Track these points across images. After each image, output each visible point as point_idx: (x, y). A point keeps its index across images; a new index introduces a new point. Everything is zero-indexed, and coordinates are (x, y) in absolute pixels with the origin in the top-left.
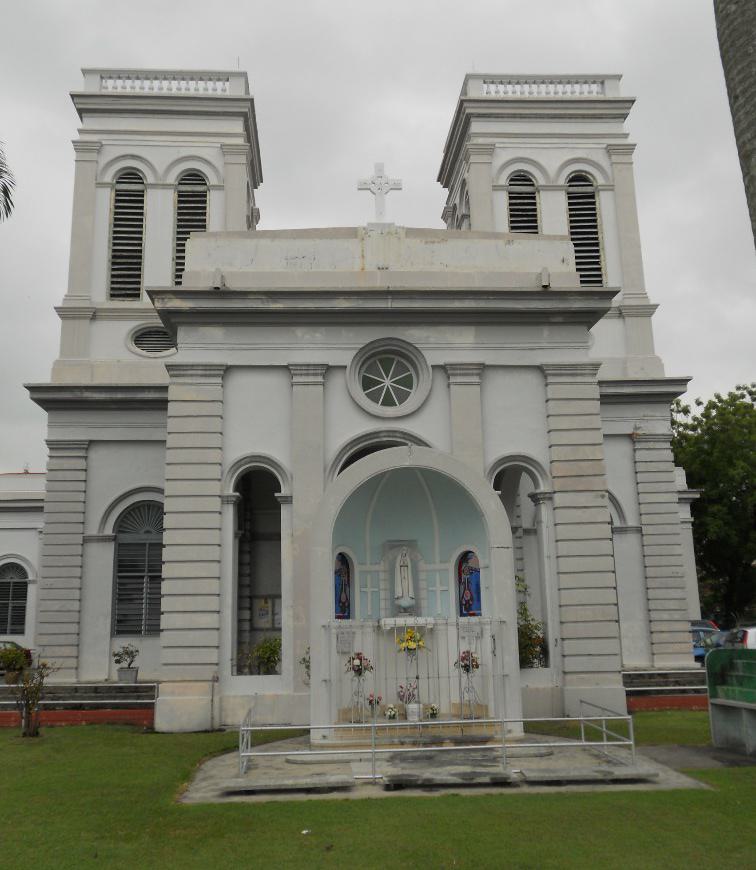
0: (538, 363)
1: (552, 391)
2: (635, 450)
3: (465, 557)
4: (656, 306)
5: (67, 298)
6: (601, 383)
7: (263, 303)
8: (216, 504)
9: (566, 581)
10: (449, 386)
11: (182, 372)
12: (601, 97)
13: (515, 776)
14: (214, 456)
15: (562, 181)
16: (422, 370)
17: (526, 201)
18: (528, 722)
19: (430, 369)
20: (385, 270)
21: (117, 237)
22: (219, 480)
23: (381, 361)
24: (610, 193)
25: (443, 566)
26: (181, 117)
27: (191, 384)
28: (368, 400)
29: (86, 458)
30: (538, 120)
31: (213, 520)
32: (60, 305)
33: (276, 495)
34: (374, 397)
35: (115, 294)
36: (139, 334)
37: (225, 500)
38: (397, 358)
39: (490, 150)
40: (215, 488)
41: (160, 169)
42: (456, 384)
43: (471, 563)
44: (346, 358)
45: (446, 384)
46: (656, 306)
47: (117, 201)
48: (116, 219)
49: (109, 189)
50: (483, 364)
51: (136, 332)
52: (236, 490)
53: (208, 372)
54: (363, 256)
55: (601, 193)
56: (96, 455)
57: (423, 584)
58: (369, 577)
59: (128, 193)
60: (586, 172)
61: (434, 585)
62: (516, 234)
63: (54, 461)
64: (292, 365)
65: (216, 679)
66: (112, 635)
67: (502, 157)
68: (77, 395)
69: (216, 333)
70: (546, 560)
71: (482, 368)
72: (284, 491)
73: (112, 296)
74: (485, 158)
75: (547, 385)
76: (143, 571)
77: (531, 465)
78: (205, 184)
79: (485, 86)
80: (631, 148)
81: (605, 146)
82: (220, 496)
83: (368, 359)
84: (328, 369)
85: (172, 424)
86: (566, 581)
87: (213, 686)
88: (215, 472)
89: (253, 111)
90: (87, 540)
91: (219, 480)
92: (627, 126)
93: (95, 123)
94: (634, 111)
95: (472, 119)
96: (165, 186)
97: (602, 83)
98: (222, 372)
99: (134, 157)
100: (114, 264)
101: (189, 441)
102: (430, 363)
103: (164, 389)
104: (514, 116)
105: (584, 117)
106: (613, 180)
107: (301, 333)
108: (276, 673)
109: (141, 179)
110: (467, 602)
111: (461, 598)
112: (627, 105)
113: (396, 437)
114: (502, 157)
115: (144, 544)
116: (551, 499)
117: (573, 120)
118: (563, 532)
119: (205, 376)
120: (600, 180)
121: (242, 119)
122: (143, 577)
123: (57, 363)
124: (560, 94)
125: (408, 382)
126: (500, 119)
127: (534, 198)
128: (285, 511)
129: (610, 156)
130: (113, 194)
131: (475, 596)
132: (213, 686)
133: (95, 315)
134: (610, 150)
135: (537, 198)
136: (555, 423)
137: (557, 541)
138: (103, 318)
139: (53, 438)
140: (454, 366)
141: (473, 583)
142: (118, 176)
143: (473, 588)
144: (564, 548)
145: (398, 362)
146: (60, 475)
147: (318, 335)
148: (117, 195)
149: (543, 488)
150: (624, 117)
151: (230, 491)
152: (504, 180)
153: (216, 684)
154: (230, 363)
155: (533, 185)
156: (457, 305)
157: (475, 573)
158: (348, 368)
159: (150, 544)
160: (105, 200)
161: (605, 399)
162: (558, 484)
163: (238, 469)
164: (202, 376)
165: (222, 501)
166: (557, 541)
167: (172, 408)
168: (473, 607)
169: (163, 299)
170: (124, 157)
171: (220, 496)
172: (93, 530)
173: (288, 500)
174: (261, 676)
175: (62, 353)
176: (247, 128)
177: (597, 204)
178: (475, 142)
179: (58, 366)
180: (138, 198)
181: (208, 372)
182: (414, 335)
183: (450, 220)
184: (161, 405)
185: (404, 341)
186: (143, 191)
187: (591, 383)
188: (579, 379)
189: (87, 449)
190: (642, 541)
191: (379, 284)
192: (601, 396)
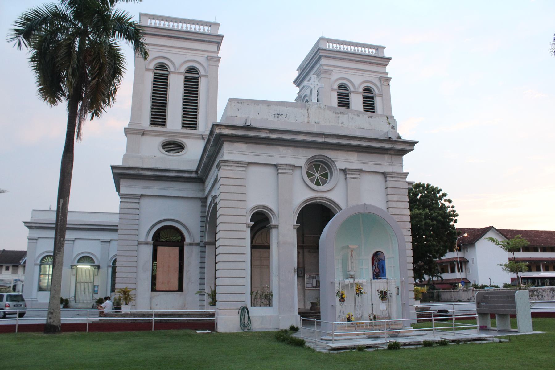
0: (383, 171)
3: (376, 254)
5: (130, 124)
7: (267, 134)
8: (244, 227)
10: (278, 174)
11: (227, 164)
12: (376, 55)
13: (312, 348)
15: (361, 90)
17: (368, 100)
18: (16, 327)
19: (338, 169)
20: (318, 124)
21: (154, 96)
23: (314, 165)
24: (381, 98)
26: (153, 37)
27: (232, 170)
28: (309, 181)
30: (351, 61)
31: (241, 235)
34: (312, 181)
35: (153, 123)
36: (165, 143)
38: (322, 164)
39: (330, 72)
41: (177, 65)
44: (302, 162)
48: (154, 87)
49: (152, 72)
50: (294, 165)
51: (163, 143)
53: (240, 165)
54: (308, 117)
55: (377, 97)
56: (144, 201)
59: (160, 75)
60: (371, 87)
63: (123, 204)
64: (279, 164)
66: (38, 291)
67: (335, 76)
69: (242, 147)
71: (361, 171)
72: (273, 222)
73: (183, 126)
74: (327, 76)
75: (386, 181)
77: (270, 212)
78: (198, 74)
81: (379, 77)
82: (245, 224)
83: (311, 163)
84: (295, 167)
90: (139, 243)
92: (388, 69)
94: (391, 62)
95: (322, 58)
96: (179, 73)
97: (377, 49)
98: (246, 165)
99: (164, 58)
100: (152, 109)
101: (230, 197)
104: (340, 59)
105: (370, 63)
106: (382, 93)
109: (167, 68)
111: (374, 271)
112: (388, 60)
113: (323, 200)
114: (335, 76)
117: (365, 64)
119: (238, 166)
120: (376, 91)
121: (217, 45)
123: (125, 156)
124: (360, 51)
125: (326, 176)
126: (335, 59)
128: (274, 232)
131: (381, 271)
133: (144, 133)
138: (147, 135)
140: (349, 170)
142: (156, 66)
145: (322, 166)
146: (126, 211)
147: (289, 151)
150: (386, 65)
152: (336, 87)
154: (250, 162)
155: (348, 90)
158: (303, 167)
160: (149, 78)
163: (253, 211)
164: (236, 166)
169: (220, 128)
171: (245, 224)
172: (142, 239)
173: (276, 227)
174: (261, 308)
175: (127, 151)
177: (375, 102)
178: (323, 68)
179: (125, 158)
180: (165, 78)
181: (240, 165)
182: (331, 155)
185: (330, 159)
186: (168, 75)
188: (399, 179)
189: (139, 199)
191: (358, 134)
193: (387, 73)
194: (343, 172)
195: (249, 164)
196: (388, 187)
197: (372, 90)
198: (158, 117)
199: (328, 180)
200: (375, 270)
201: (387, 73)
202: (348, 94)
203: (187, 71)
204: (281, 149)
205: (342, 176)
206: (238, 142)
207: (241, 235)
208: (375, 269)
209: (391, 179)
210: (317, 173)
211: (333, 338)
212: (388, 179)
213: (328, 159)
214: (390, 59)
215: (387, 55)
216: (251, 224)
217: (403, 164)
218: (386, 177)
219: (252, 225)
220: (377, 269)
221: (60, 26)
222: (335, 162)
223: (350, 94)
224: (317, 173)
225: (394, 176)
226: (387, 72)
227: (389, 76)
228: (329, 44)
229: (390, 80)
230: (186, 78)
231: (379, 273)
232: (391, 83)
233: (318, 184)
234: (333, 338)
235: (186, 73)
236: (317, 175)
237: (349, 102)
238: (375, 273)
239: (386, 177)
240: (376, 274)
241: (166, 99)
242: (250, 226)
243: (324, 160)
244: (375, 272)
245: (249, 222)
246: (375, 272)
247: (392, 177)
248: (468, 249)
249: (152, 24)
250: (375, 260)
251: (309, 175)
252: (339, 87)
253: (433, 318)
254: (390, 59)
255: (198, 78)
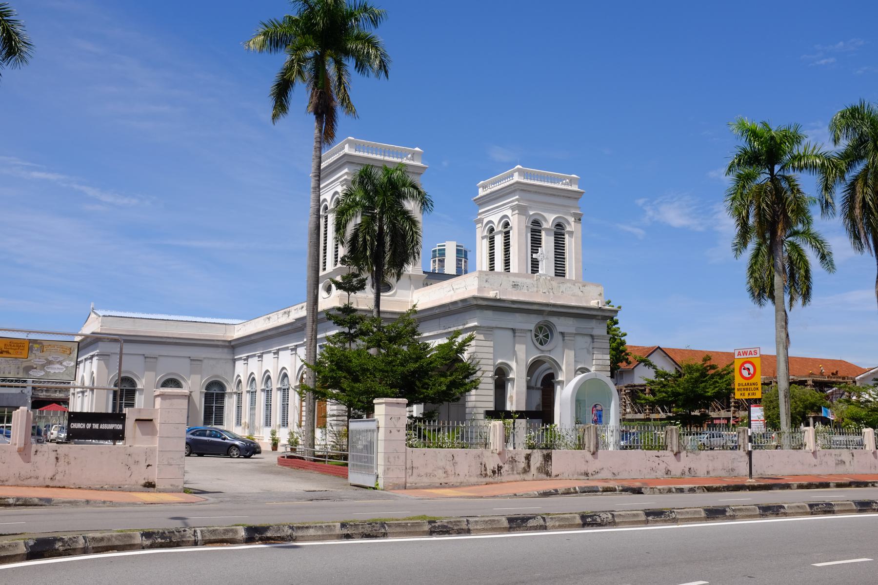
34: (537, 340)
44: (532, 327)
119: (487, 330)
182: (554, 320)
185: (554, 325)
194: (591, 338)
195: (493, 328)
197: (563, 225)
199: (549, 340)
204: (517, 315)
205: (560, 337)
206: (486, 310)
209: (520, 335)
212: (595, 340)
213: (552, 324)
218: (564, 337)
221: (418, 151)
233: (541, 344)
239: (564, 337)
248: (624, 375)
251: (536, 336)
252: (532, 222)
253: (124, 402)
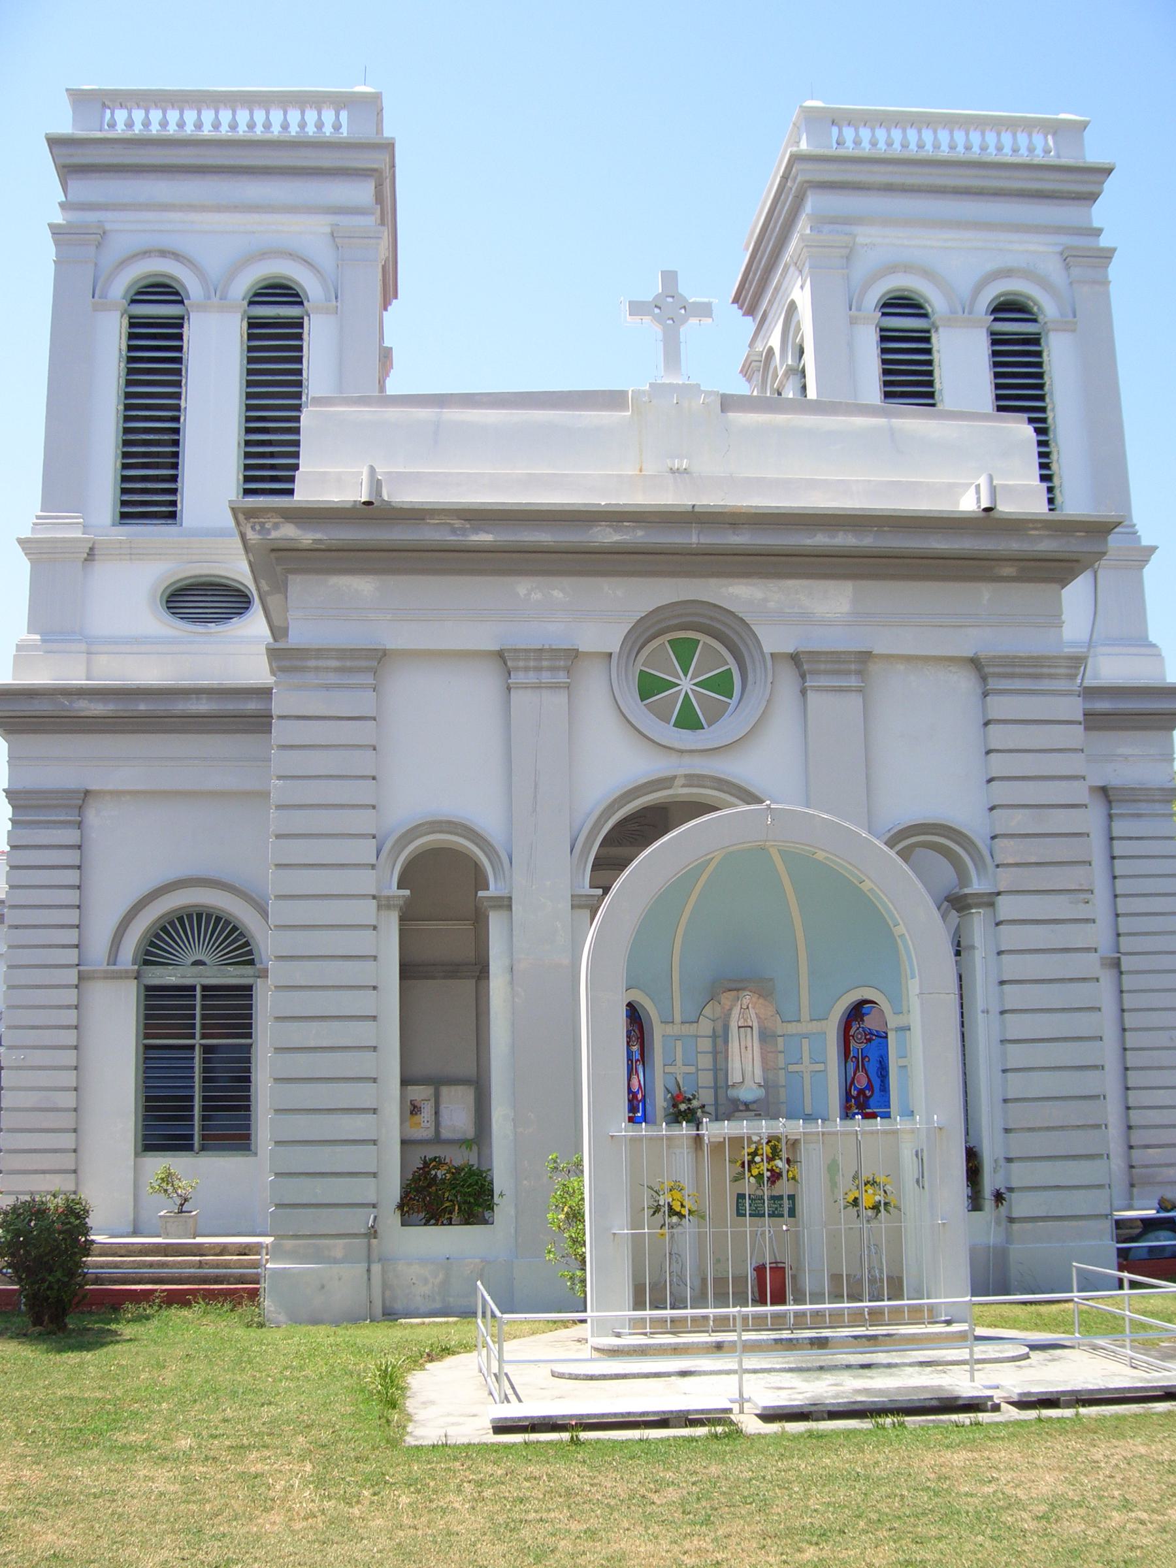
1: (1000, 706)
2: (1110, 817)
3: (857, 1011)
4: (1152, 549)
6: (1090, 693)
8: (367, 911)
9: (1018, 1056)
10: (803, 692)
14: (362, 821)
16: (754, 670)
19: (768, 658)
22: (373, 867)
25: (814, 1027)
29: (79, 825)
31: (361, 942)
32: (27, 534)
33: (481, 894)
37: (383, 903)
40: (366, 882)
42: (819, 689)
43: (870, 1022)
45: (979, 691)
46: (1152, 549)
47: (131, 336)
52: (400, 886)
57: (705, 1061)
58: (805, 1042)
61: (799, 1061)
62: (894, 406)
64: (509, 650)
65: (373, 1233)
68: (159, 707)
70: (981, 1017)
72: (494, 889)
75: (985, 694)
76: (193, 1036)
79: (835, 130)
80: (1107, 255)
82: (374, 897)
85: (281, 761)
86: (1018, 1056)
87: (369, 1245)
88: (365, 851)
89: (393, 166)
91: (373, 867)
92: (1099, 213)
93: (89, 189)
94: (1110, 185)
102: (768, 649)
103: (264, 693)
107: (525, 588)
108: (485, 1222)
110: (861, 1092)
115: (193, 988)
116: (992, 905)
118: (1013, 967)
122: (192, 1047)
127: (928, 340)
128: (496, 923)
129: (1068, 267)
130: (125, 322)
132: (369, 1245)
134: (1068, 258)
135: (934, 340)
136: (999, 765)
137: (1002, 983)
139: (19, 786)
140: (814, 655)
141: (873, 1056)
143: (873, 1067)
144: (1015, 996)
148: (132, 325)
149: (977, 886)
150: (1092, 197)
151: (392, 889)
153: (374, 1241)
155: (925, 316)
156: (821, 540)
157: (876, 1040)
159: (205, 988)
161: (1094, 721)
162: (1005, 878)
165: (379, 907)
166: (1002, 983)
167: (280, 732)
168: (872, 1101)
170: (146, 253)
171: (374, 897)
173: (505, 904)
176: (379, 198)
177: (1045, 354)
183: (758, 377)
184: (261, 723)
185: (732, 613)
187: (1067, 693)
188: (1045, 684)
190: (1120, 984)
192: (1086, 715)
193: (1098, 232)
196: (990, 718)
198: (149, 485)
200: (852, 1082)
201: (1098, 232)
202: (928, 331)
203: (257, 295)
207: (361, 942)
208: (855, 1074)
210: (686, 675)
211: (740, 1336)
214: (1108, 171)
215: (1093, 156)
216: (399, 897)
217: (1064, 617)
219: (401, 902)
220: (860, 1073)
222: (753, 627)
223: (933, 331)
224: (686, 675)
225: (1017, 670)
226: (1096, 224)
227: (1104, 241)
228: (112, 114)
229: (1111, 258)
230: (253, 324)
231: (868, 1093)
232: (1114, 271)
234: (740, 1336)
235: (251, 303)
236: (686, 685)
237: (930, 363)
238: (854, 1093)
240: (858, 1094)
241: (176, 413)
242: (394, 906)
243: (708, 622)
244: (856, 1088)
245: (393, 890)
246: (856, 1088)
247: (1012, 676)
249: (942, 148)
250: (853, 1036)
254: (1108, 171)
255: (303, 318)
